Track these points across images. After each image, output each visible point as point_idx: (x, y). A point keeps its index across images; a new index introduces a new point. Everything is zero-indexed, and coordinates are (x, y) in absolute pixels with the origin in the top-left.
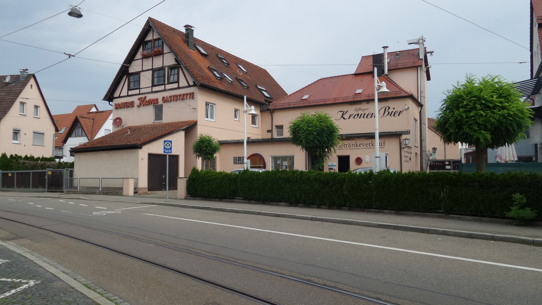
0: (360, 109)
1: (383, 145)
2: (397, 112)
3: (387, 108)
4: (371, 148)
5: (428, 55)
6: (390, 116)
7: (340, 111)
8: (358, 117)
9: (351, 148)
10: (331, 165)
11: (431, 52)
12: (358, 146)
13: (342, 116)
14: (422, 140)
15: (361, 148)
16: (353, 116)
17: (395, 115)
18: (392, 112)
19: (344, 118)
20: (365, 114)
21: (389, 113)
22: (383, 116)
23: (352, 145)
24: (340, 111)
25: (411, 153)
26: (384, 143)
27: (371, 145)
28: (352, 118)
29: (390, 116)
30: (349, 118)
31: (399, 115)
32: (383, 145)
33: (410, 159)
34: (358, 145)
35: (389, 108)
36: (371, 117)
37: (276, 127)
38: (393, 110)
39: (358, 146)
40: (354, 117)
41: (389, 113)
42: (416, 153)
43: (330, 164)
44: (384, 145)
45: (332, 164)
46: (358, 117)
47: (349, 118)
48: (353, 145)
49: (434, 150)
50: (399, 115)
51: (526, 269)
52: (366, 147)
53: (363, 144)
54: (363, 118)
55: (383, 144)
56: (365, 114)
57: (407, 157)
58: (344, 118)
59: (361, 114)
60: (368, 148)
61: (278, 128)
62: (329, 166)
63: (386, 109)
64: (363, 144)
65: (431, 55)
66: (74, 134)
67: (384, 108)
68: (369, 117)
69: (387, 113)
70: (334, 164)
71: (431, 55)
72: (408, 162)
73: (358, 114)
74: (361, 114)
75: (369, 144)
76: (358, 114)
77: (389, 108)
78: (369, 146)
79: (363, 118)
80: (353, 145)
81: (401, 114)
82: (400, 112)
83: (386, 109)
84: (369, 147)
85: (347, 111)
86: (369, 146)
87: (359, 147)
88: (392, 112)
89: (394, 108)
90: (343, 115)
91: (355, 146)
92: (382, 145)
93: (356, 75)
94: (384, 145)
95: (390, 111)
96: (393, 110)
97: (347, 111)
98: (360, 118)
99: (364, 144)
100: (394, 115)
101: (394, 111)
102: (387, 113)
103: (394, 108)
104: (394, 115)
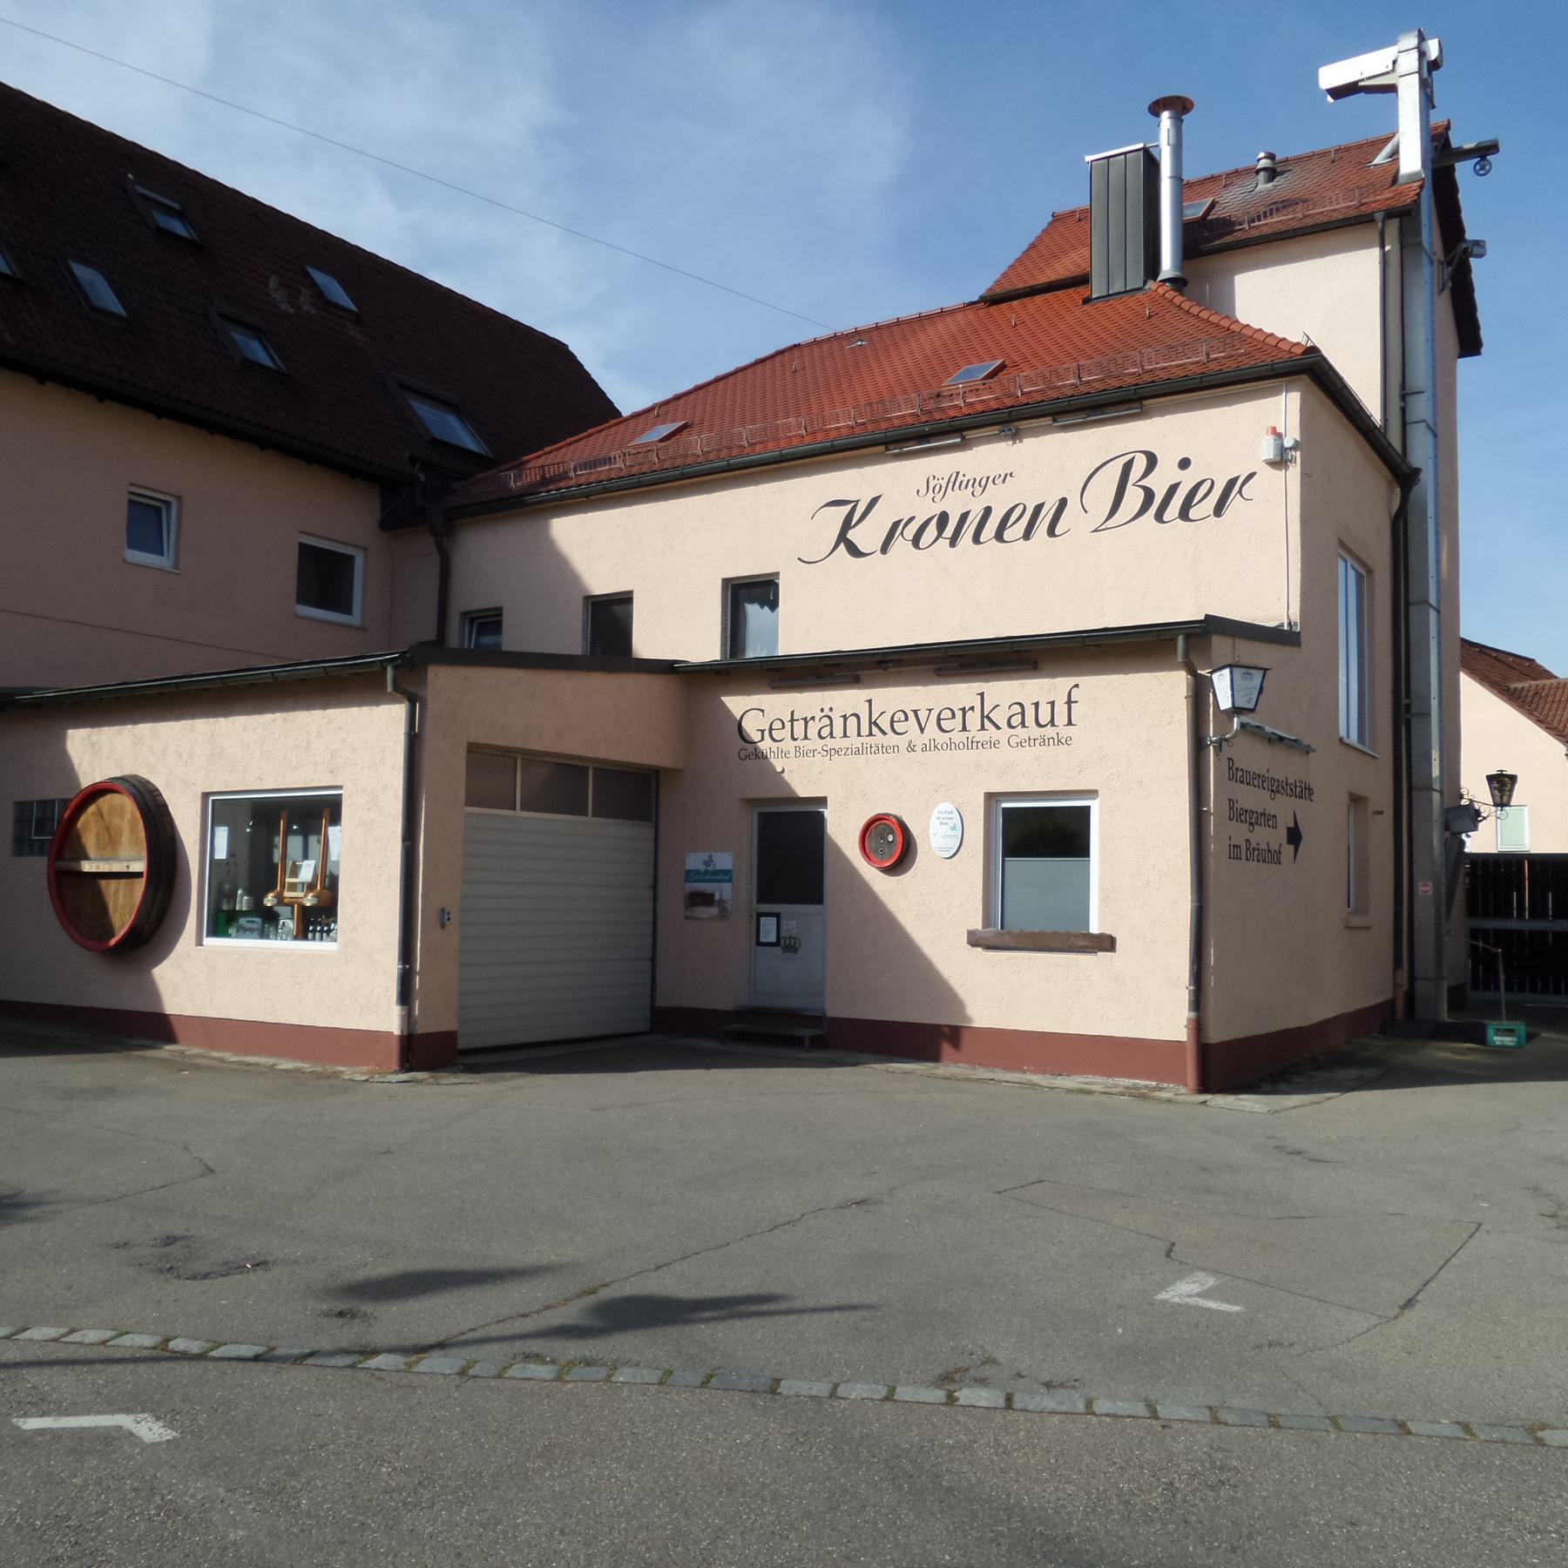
0: (955, 482)
1: (1061, 718)
2: (1208, 483)
3: (1140, 464)
4: (972, 744)
5: (1464, 172)
6: (1159, 517)
7: (825, 506)
8: (939, 535)
9: (838, 742)
10: (702, 868)
11: (1485, 151)
12: (887, 728)
13: (842, 538)
14: (1414, 710)
15: (902, 741)
16: (910, 531)
17: (1192, 514)
18: (1173, 489)
19: (854, 551)
20: (988, 511)
21: (1149, 494)
22: (1110, 523)
23: (845, 717)
24: (825, 506)
25: (1305, 792)
26: (1069, 702)
27: (974, 719)
28: (901, 545)
29: (1159, 517)
30: (884, 549)
31: (1219, 510)
32: (1061, 718)
33: (1294, 836)
34: (884, 722)
35: (1152, 460)
36: (1027, 535)
37: (472, 620)
38: (1178, 475)
39: (887, 728)
40: (916, 542)
41: (1149, 494)
42: (1356, 800)
43: (695, 861)
44: (1070, 723)
45: (707, 863)
46: (939, 535)
47: (884, 549)
48: (852, 721)
49: (1501, 791)
50: (1219, 510)
51: (1432, 670)
52: (942, 738)
53: (915, 712)
54: (976, 539)
55: (1061, 709)
56: (988, 511)
57: (1268, 819)
58: (854, 551)
59: (964, 517)
60: (950, 745)
61: (481, 626)
62: (690, 875)
63: (1128, 467)
64: (915, 712)
65: (1483, 170)
66: (784, 795)
67: (1115, 470)
68: (1015, 531)
69: (1134, 498)
70: (724, 861)
71: (1483, 170)
72: (1273, 857)
73: (943, 519)
74: (964, 517)
75: (959, 714)
76: (943, 519)
77: (1152, 460)
78: (964, 729)
79: (976, 539)
80: (852, 721)
81: (1235, 502)
82: (1231, 483)
83: (1128, 467)
84: (958, 737)
85: (874, 501)
86: (964, 729)
87: (892, 739)
88: (1173, 489)
89: (1184, 464)
90: (847, 525)
91: (865, 730)
92: (1052, 722)
93: (992, 300)
94: (1070, 723)
95: (1159, 483)
96: (1178, 475)
97: (874, 501)
98: (953, 542)
99: (923, 715)
100: (1184, 514)
101: (1188, 480)
102: (1134, 498)
103: (1184, 464)
104: (1184, 514)
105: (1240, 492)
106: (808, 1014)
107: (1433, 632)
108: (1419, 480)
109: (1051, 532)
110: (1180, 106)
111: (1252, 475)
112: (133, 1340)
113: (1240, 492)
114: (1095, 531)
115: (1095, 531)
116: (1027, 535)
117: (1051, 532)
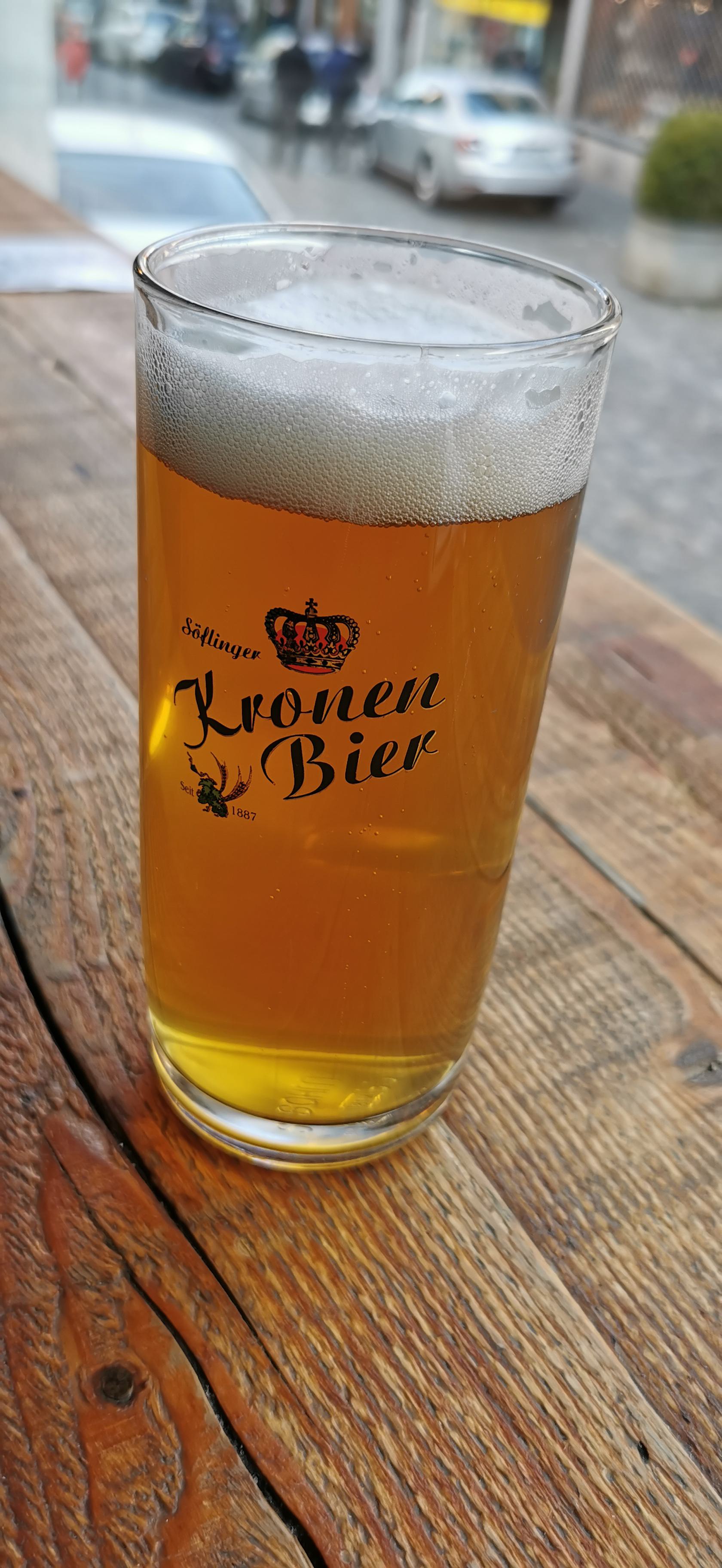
16: (265, 708)
31: (408, 764)
36: (401, 708)
50: (408, 764)
69: (313, 775)
81: (420, 757)
82: (414, 742)
102: (313, 775)
105: (423, 747)
106: (397, 1449)
107: (380, 1058)
108: (114, 1100)
109: (425, 702)
110: (423, 554)
111: (431, 733)
112: (629, 1260)
113: (423, 747)
114: (287, 798)
115: (287, 798)
116: (401, 708)
117: (425, 702)
